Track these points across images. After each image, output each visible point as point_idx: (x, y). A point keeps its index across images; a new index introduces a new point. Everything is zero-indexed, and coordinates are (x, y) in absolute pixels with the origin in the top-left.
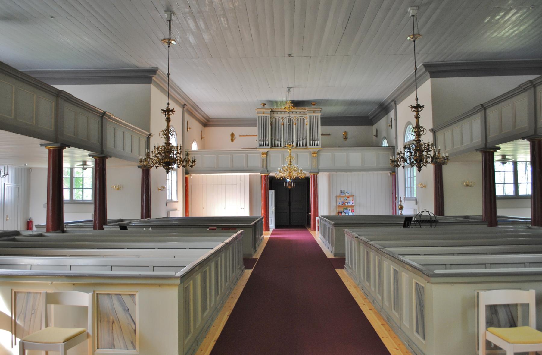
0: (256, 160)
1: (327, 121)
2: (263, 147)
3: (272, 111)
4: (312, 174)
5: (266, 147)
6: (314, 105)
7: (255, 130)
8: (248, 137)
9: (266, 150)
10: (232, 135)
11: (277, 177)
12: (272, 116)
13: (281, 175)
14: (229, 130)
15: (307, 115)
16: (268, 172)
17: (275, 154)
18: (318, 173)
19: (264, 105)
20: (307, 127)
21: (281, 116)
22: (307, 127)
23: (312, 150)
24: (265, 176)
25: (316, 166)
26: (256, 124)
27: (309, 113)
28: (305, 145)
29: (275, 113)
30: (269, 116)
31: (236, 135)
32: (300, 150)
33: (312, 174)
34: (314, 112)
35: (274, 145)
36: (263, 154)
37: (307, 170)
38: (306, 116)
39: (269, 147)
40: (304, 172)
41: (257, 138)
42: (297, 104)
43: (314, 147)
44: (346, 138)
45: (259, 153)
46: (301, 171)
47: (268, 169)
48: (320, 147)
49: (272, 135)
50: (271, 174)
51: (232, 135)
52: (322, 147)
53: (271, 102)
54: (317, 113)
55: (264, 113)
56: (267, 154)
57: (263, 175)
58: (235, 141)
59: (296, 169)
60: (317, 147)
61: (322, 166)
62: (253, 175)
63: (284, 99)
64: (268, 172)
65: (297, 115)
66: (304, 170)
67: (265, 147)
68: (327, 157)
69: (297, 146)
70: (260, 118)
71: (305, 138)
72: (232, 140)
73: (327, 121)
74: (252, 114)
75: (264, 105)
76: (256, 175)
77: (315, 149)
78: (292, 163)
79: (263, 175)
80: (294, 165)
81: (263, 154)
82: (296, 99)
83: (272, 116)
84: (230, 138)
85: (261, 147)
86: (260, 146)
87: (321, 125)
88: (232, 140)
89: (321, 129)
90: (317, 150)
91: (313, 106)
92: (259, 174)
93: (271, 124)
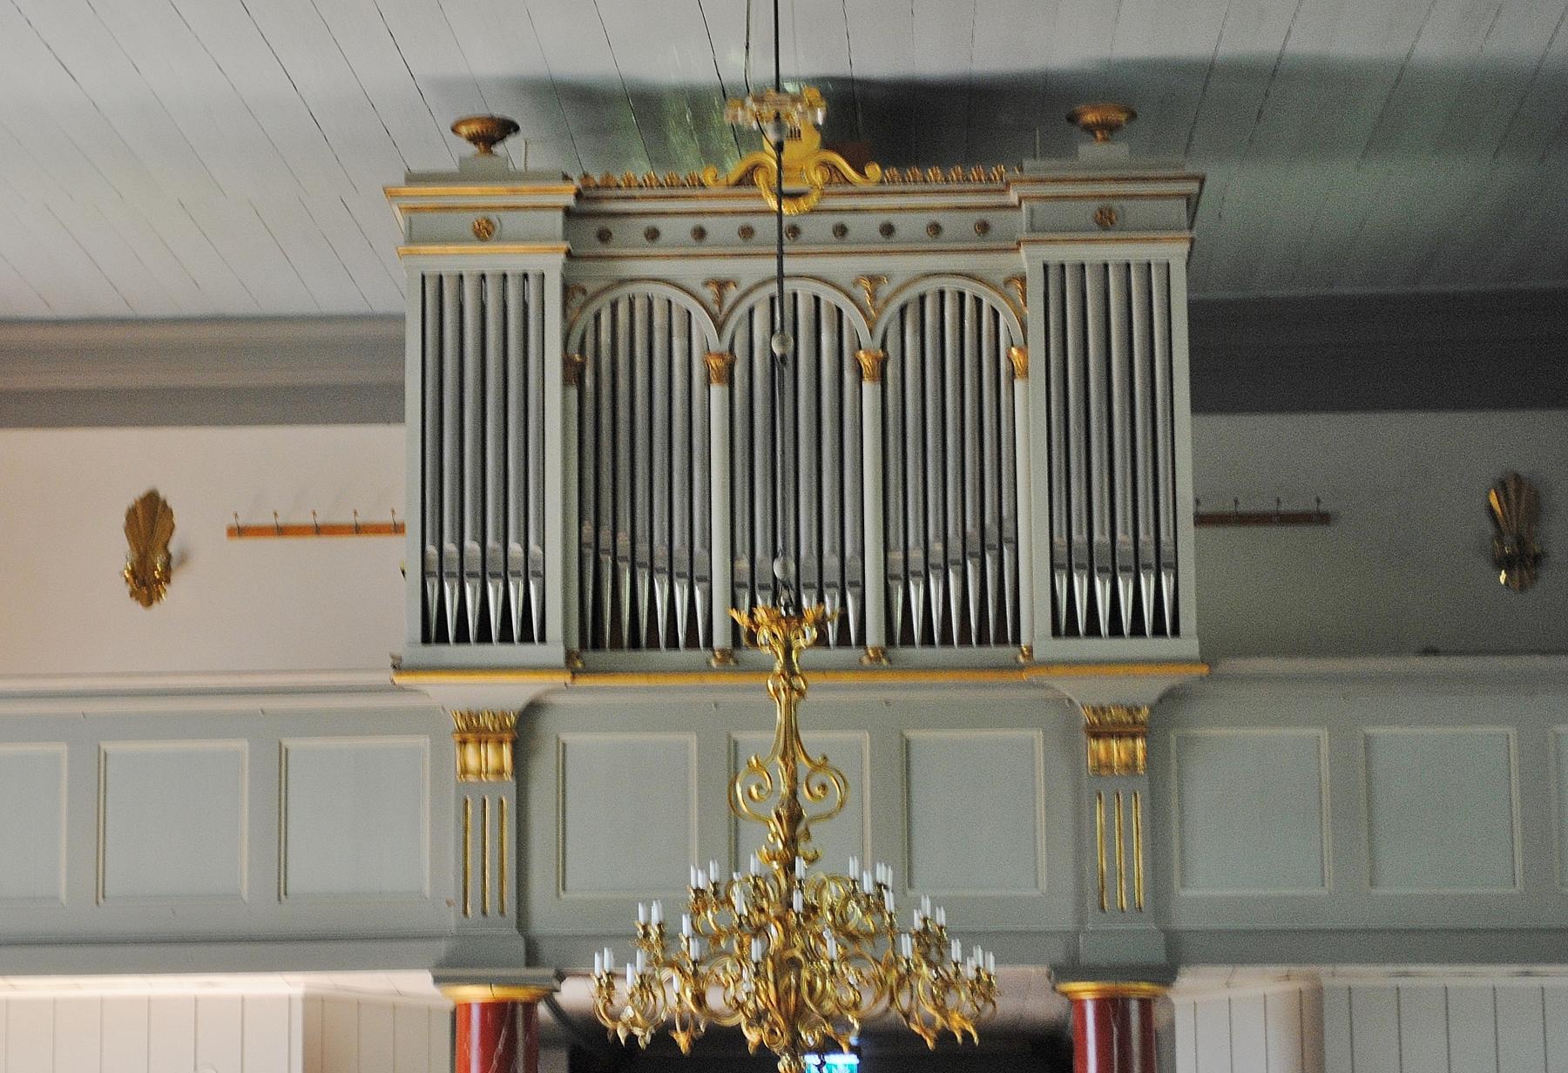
0: (395, 831)
1: (1263, 346)
2: (473, 652)
3: (588, 217)
4: (1087, 991)
5: (517, 652)
6: (1109, 129)
7: (378, 463)
8: (312, 531)
9: (511, 692)
10: (150, 520)
11: (628, 1019)
12: (593, 276)
13: (674, 994)
14: (123, 460)
15: (1027, 260)
16: (532, 957)
17: (618, 730)
18: (1165, 975)
19: (494, 132)
20: (1027, 406)
21: (695, 271)
22: (1027, 406)
23: (1087, 692)
24: (499, 1015)
25: (1132, 887)
26: (399, 390)
27: (1040, 232)
28: (996, 626)
29: (629, 234)
30: (551, 263)
31: (191, 529)
32: (930, 686)
33: (1087, 991)
34: (1106, 221)
35: (605, 633)
36: (473, 730)
37: (1007, 944)
38: (992, 254)
39: (553, 650)
40: (978, 962)
41: (405, 551)
42: (888, 124)
43: (1104, 647)
44: (1522, 557)
45: (423, 720)
46: (931, 943)
47: (541, 922)
48: (1187, 644)
49: (595, 499)
50: (576, 994)
51: (150, 520)
52: (1210, 655)
53: (590, 107)
54: (1154, 230)
55: (484, 232)
56: (523, 731)
57: (476, 994)
58: (176, 593)
59: (856, 915)
60: (1150, 646)
61: (1219, 876)
62: (359, 1005)
63: (737, 63)
64: (532, 957)
65: (886, 248)
66: (971, 939)
67: (496, 652)
68: (1264, 791)
69: (898, 635)
70: (434, 290)
71: (995, 540)
72: (147, 581)
73: (1263, 346)
74: (370, 274)
75: (494, 132)
76: (395, 1009)
77: (1127, 672)
78: (820, 837)
79: (476, 994)
80: (848, 864)
81: (473, 730)
82: (878, 61)
83: (593, 276)
84: (119, 553)
85: (452, 652)
86: (434, 632)
87: (1199, 405)
88: (147, 581)
89: (1194, 449)
90: (1144, 689)
91: (1092, 151)
92: (417, 984)
93: (573, 373)
